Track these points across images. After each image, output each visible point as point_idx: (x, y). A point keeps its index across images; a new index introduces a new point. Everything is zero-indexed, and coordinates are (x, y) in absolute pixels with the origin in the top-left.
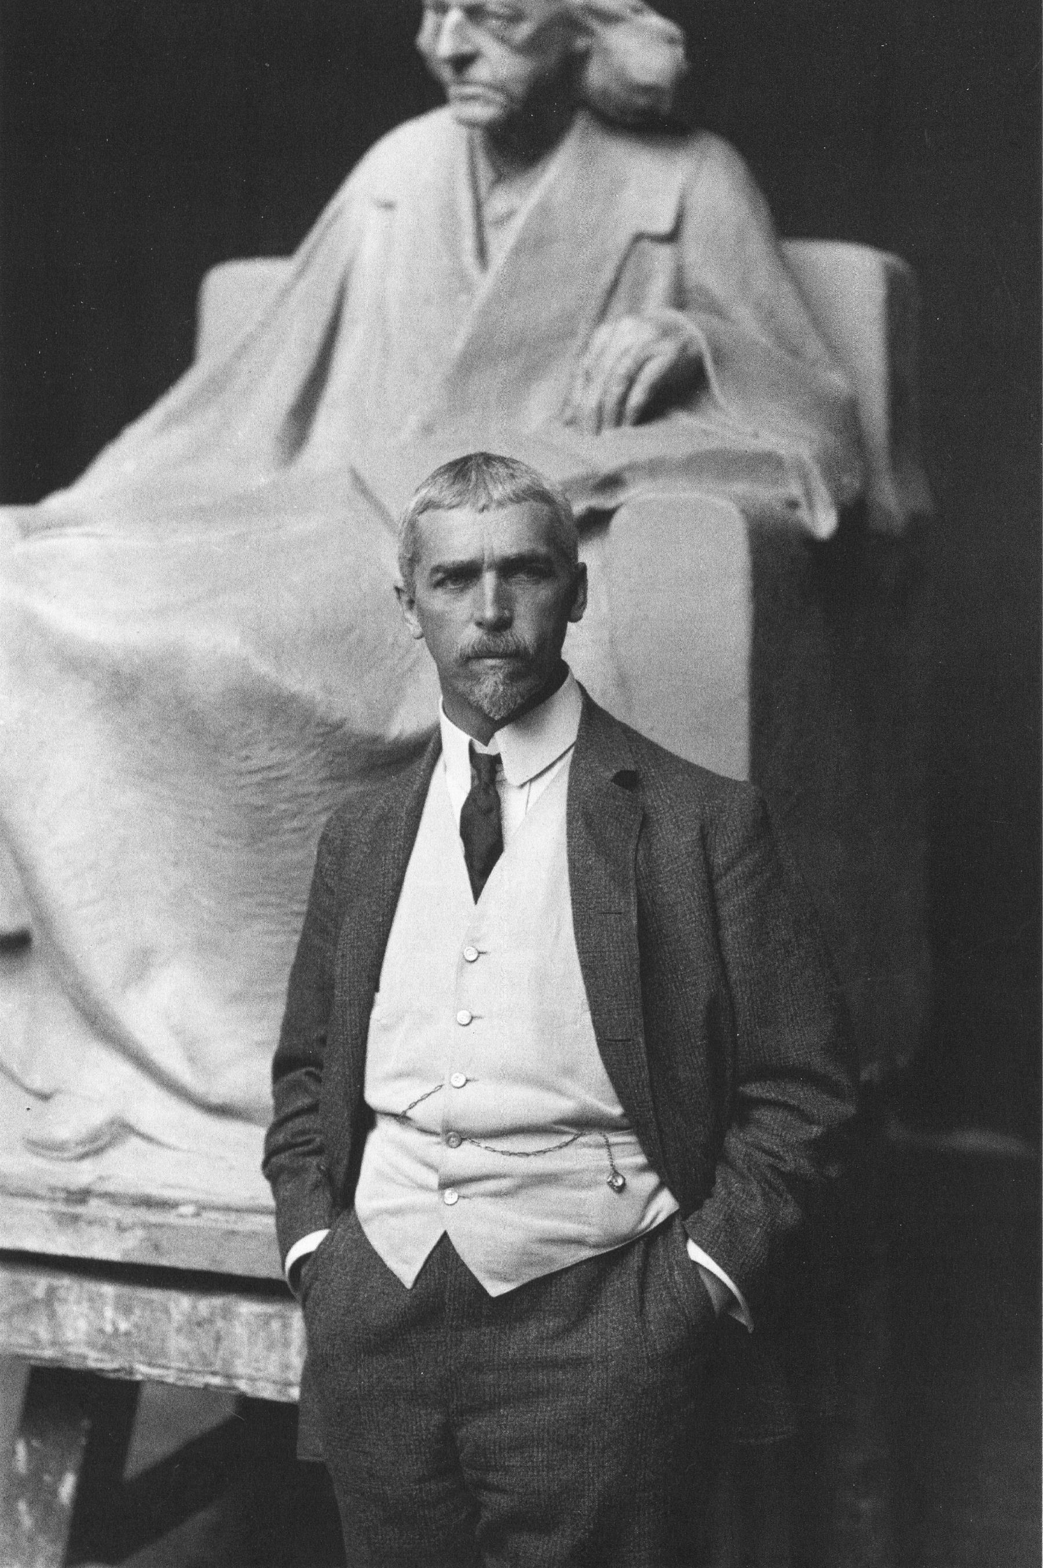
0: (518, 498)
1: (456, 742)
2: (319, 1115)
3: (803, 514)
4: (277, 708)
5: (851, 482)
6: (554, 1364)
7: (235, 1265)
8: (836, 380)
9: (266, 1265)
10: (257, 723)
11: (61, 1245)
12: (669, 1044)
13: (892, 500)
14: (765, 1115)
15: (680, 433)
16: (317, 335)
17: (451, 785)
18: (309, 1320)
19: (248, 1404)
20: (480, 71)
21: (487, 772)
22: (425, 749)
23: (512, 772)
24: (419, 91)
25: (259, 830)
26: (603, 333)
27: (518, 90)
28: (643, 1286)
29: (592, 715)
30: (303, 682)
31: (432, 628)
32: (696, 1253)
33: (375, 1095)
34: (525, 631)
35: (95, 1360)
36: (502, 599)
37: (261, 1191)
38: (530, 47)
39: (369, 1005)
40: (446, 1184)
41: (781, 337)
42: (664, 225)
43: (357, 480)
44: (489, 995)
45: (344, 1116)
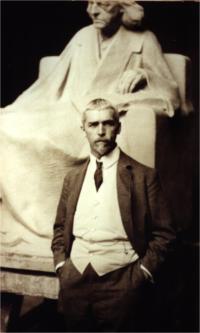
0: (107, 108)
1: (93, 159)
2: (63, 236)
3: (167, 112)
4: (56, 152)
5: (177, 105)
6: (113, 291)
7: (45, 269)
8: (174, 84)
9: (52, 269)
10: (51, 155)
11: (7, 265)
12: (137, 222)
13: (186, 109)
14: (157, 238)
15: (142, 94)
16: (65, 73)
17: (92, 168)
18: (60, 281)
19: (47, 301)
20: (100, 17)
21: (100, 165)
22: (85, 162)
23: (104, 166)
24: (87, 21)
25: (52, 177)
26: (126, 73)
27: (108, 21)
28: (131, 274)
29: (122, 155)
30: (61, 146)
31: (88, 136)
32: (142, 267)
33: (75, 233)
34: (108, 136)
35: (14, 291)
36: (104, 130)
37: (50, 253)
38: (111, 11)
39: (74, 214)
40: (90, 252)
41: (163, 74)
42: (139, 50)
43: (73, 105)
44: (100, 216)
45: (68, 237)
